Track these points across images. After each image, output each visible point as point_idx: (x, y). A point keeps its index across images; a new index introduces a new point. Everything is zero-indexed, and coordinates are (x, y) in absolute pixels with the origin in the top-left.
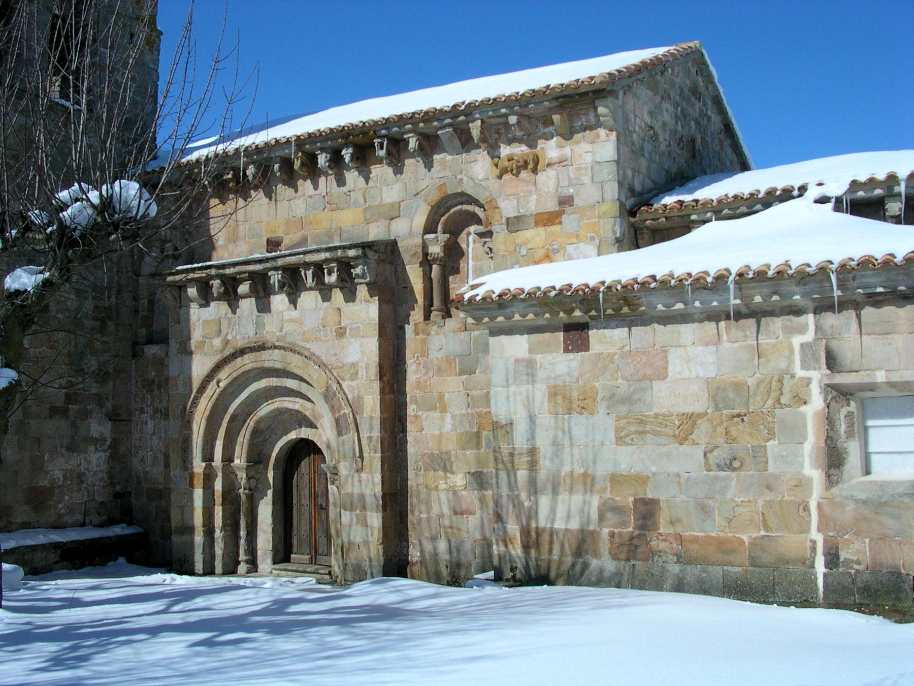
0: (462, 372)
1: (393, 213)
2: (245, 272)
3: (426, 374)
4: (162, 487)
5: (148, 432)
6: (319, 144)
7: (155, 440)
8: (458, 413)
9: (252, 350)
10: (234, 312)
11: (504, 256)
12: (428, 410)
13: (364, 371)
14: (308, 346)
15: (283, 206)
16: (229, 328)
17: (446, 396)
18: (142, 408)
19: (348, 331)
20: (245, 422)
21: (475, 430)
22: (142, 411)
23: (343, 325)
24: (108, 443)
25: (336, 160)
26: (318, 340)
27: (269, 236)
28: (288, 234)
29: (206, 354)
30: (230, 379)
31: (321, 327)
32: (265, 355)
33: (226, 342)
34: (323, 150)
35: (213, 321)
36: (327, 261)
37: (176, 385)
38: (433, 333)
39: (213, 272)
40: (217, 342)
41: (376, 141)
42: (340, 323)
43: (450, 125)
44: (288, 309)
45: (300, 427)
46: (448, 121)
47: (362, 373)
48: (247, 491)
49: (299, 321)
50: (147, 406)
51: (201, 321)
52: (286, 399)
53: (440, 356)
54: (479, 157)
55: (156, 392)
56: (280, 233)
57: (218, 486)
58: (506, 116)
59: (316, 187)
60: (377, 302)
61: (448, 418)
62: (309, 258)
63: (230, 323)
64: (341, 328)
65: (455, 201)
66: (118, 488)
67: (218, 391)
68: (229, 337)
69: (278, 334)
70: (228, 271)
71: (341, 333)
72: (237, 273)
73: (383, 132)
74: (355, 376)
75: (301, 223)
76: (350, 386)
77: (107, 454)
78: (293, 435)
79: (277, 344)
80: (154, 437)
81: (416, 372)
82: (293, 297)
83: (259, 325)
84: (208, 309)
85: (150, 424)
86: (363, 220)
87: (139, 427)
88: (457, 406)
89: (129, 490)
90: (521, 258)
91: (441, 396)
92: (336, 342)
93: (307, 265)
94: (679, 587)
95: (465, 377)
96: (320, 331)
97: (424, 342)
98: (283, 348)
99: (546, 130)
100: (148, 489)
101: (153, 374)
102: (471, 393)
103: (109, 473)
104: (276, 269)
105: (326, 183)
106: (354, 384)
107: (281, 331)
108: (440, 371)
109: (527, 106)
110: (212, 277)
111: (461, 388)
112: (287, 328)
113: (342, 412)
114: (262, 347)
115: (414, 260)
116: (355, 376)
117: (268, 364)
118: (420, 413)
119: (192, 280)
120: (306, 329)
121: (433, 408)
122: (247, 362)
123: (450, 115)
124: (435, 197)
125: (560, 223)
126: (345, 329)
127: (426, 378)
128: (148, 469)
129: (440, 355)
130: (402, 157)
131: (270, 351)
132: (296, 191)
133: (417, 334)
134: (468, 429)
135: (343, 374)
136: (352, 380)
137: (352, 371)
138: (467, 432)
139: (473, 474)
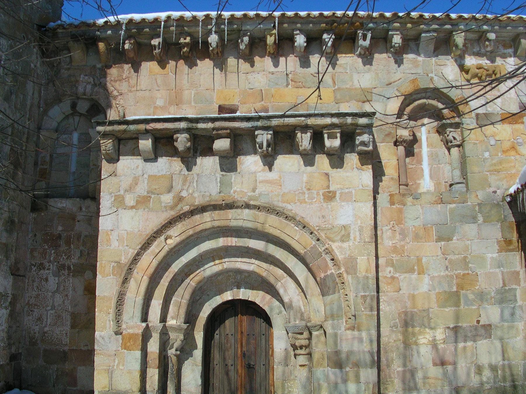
0: (440, 239)
1: (366, 96)
2: (226, 129)
3: (403, 239)
4: (66, 348)
5: (53, 288)
6: (299, 25)
7: (58, 299)
8: (436, 275)
9: (216, 207)
10: (189, 169)
11: (475, 144)
12: (406, 273)
13: (358, 234)
14: (289, 207)
15: (232, 77)
16: (184, 184)
17: (424, 260)
18: (41, 264)
19: (338, 195)
20: (183, 281)
21: (455, 289)
22: (41, 267)
23: (332, 189)
24: (9, 299)
25: (314, 40)
26: (303, 202)
27: (221, 103)
28: (245, 103)
29: (151, 210)
30: (183, 237)
31: (305, 190)
32: (231, 213)
33: (180, 199)
34: (302, 31)
35: (163, 176)
36: (333, 126)
37: (109, 240)
38: (409, 204)
39: (183, 125)
40: (167, 199)
41: (360, 33)
42: (328, 187)
43: (435, 30)
44: (263, 170)
45: (239, 288)
46: (435, 26)
47: (355, 234)
48: (178, 352)
49: (278, 183)
50: (50, 262)
51: (146, 176)
52: (239, 259)
53: (416, 224)
54: (448, 62)
55: (63, 248)
56: (235, 101)
57: (153, 346)
58: (487, 31)
59: (276, 65)
60: (371, 170)
61: (426, 279)
62: (311, 121)
63: (185, 181)
64: (330, 192)
65: (419, 96)
66: (13, 350)
67: (167, 249)
68: (184, 194)
69: (249, 194)
70: (201, 126)
71: (330, 196)
72: (214, 129)
73: (371, 25)
74: (346, 238)
75: (261, 95)
76: (341, 247)
77: (8, 311)
78: (228, 296)
79: (252, 203)
80: (57, 296)
81: (392, 238)
82: (270, 159)
83: (224, 184)
84: (155, 163)
85: (53, 282)
86: (333, 99)
87: (35, 284)
88: (437, 270)
89: (20, 351)
90: (490, 147)
91: (419, 260)
92: (325, 205)
93: (305, 128)
94: (31, 391)
95: (443, 243)
96: (304, 193)
97: (400, 211)
98: (258, 208)
99: (505, 51)
100: (45, 351)
101: (60, 228)
102: (449, 257)
103: (8, 332)
104: (266, 128)
105: (290, 63)
106: (345, 245)
107: (254, 190)
108: (417, 237)
109: (506, 27)
110: (178, 131)
111: (439, 253)
112: (261, 189)
113: (329, 272)
114: (231, 206)
115: (388, 139)
116: (346, 238)
117: (234, 223)
118: (397, 275)
119: (147, 131)
120: (286, 191)
121: (411, 271)
122: (207, 220)
123: (439, 22)
124: (408, 88)
125: (523, 123)
126: (334, 193)
127: (402, 243)
128: (46, 329)
129: (417, 223)
130: (373, 51)
131: (239, 211)
132: (252, 65)
133: (392, 203)
134: (447, 289)
135: (332, 236)
136: (343, 241)
137: (343, 232)
138: (445, 292)
139: (453, 328)
